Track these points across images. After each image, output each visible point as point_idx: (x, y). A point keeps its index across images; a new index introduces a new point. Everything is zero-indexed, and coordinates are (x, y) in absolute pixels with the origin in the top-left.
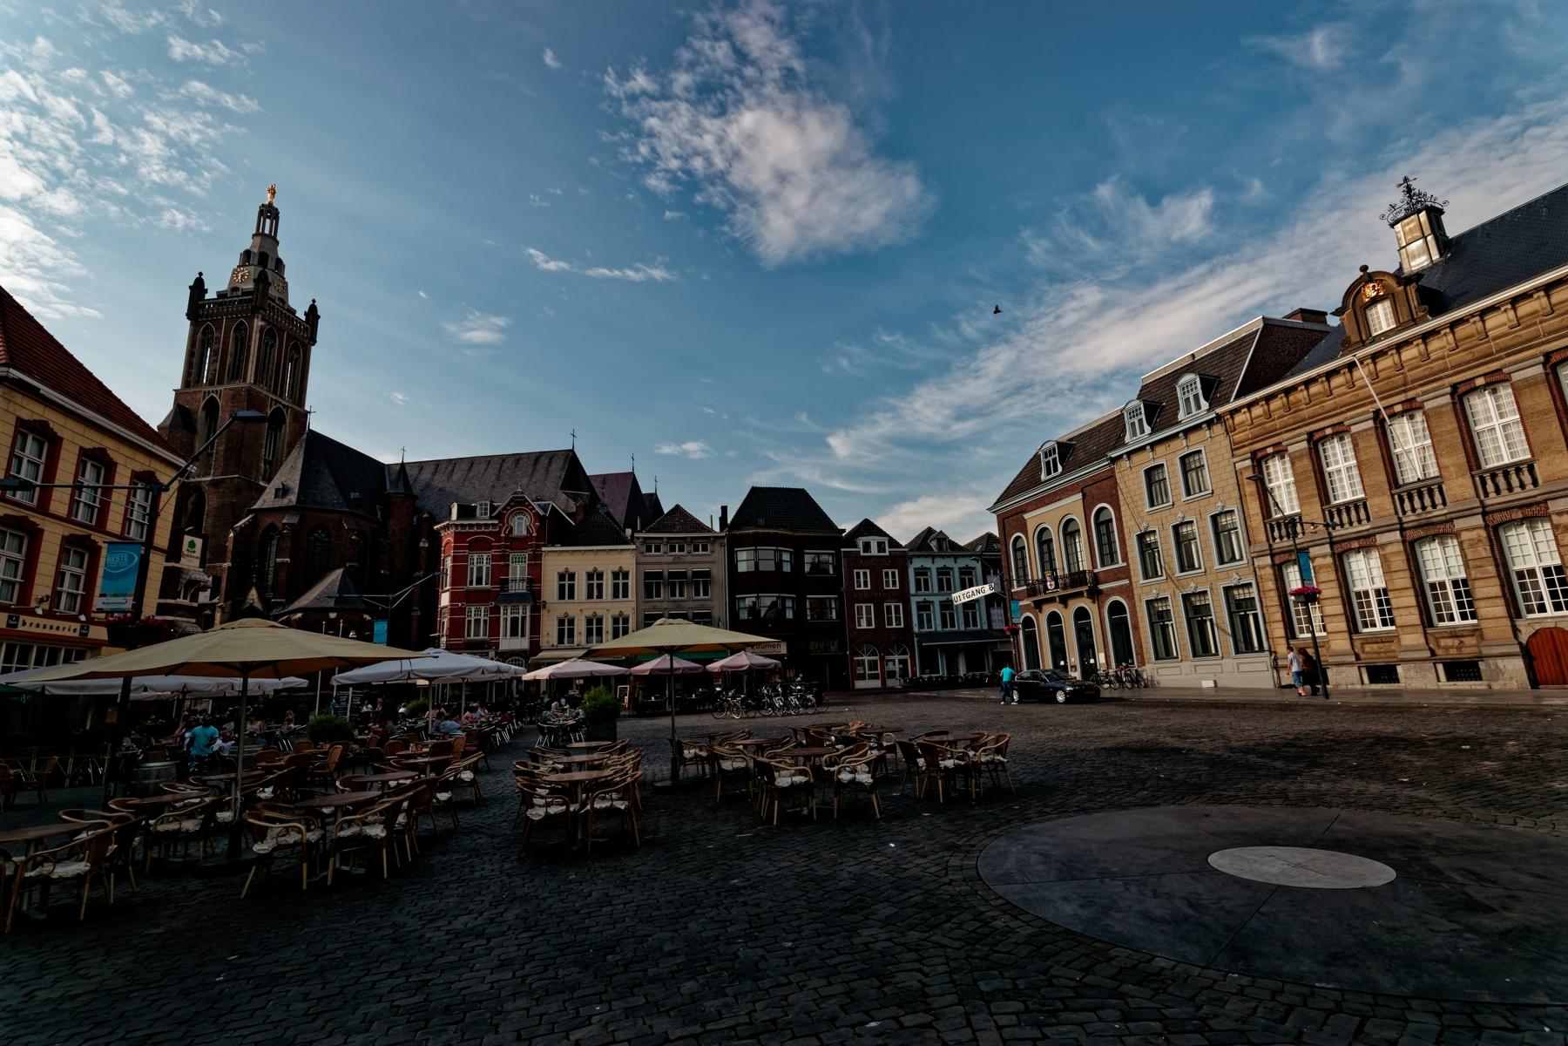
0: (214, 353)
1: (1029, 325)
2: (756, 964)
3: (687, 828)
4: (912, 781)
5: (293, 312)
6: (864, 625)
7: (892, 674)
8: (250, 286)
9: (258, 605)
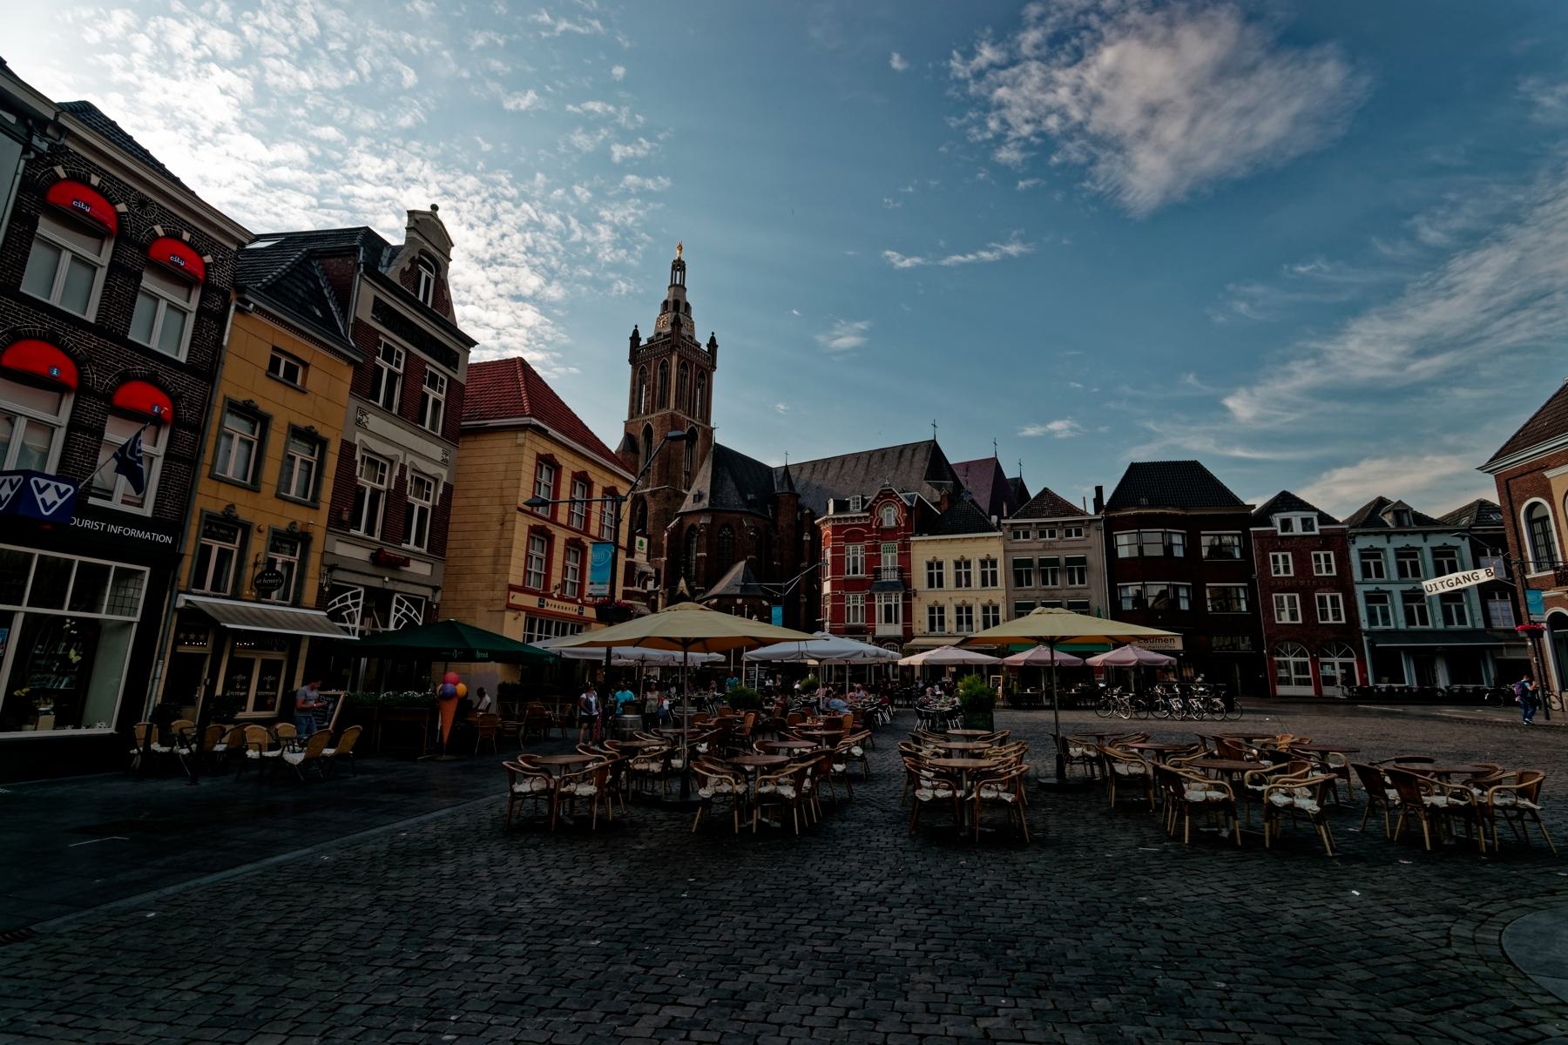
0: (648, 388)
1: (1539, 211)
2: (1181, 998)
3: (1080, 831)
4: (1379, 817)
5: (698, 345)
6: (1286, 619)
7: (1330, 681)
8: (668, 330)
9: (686, 592)
